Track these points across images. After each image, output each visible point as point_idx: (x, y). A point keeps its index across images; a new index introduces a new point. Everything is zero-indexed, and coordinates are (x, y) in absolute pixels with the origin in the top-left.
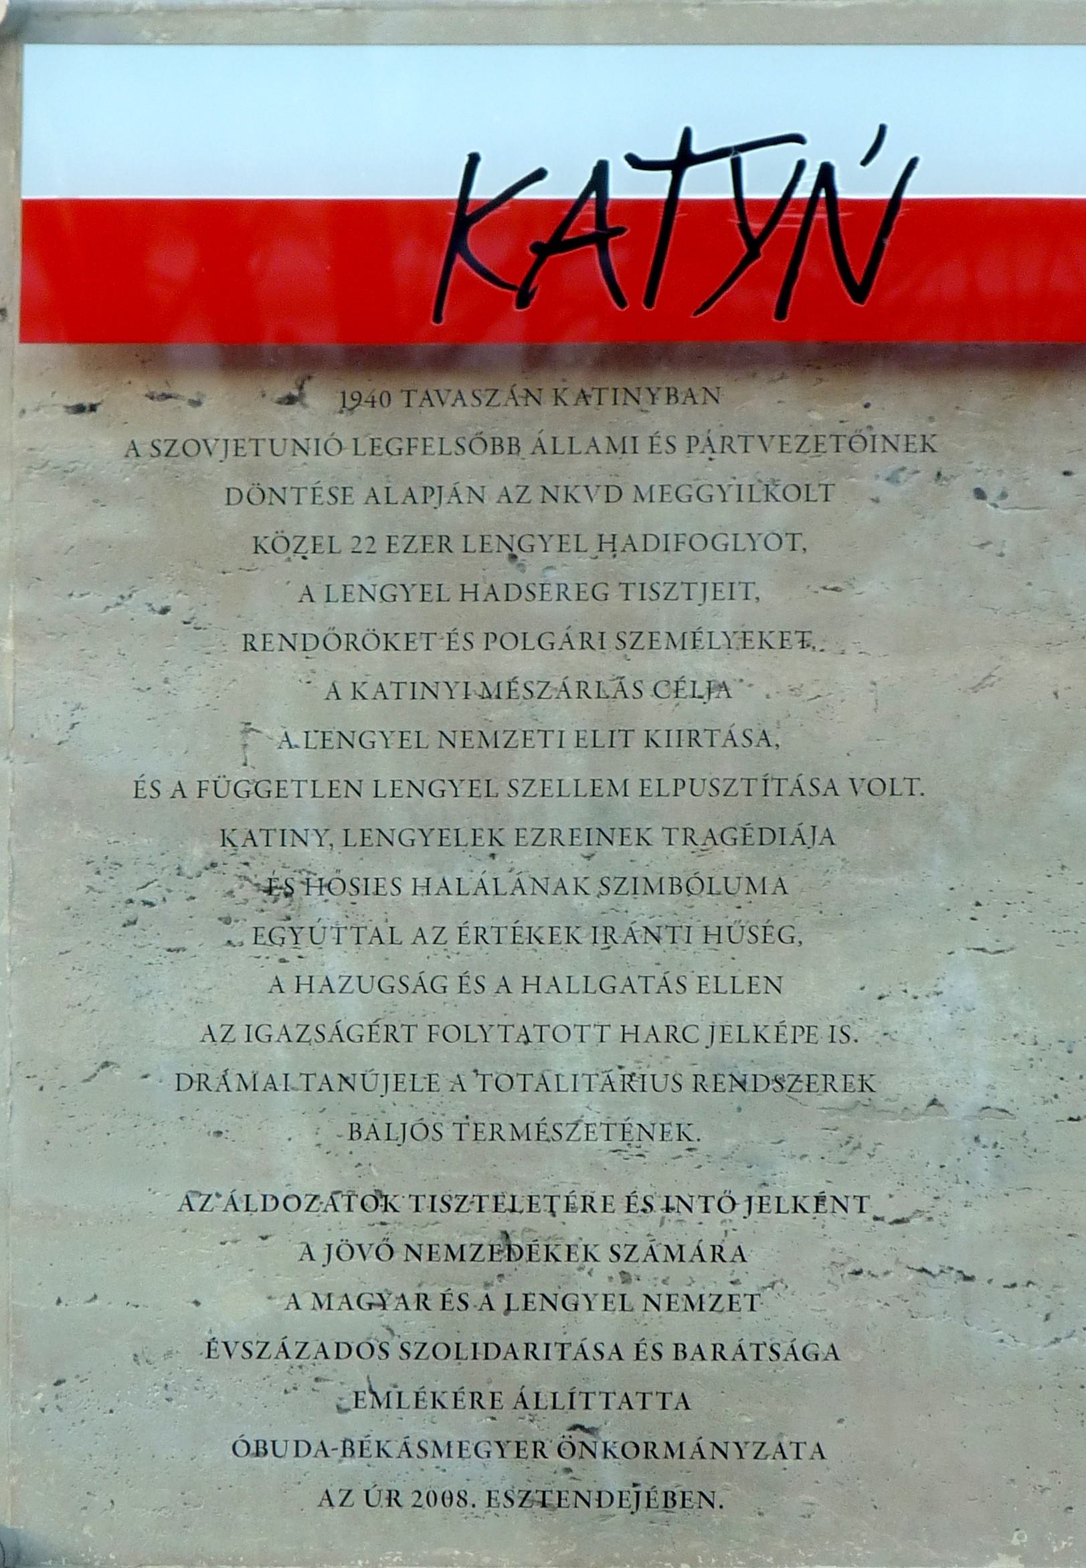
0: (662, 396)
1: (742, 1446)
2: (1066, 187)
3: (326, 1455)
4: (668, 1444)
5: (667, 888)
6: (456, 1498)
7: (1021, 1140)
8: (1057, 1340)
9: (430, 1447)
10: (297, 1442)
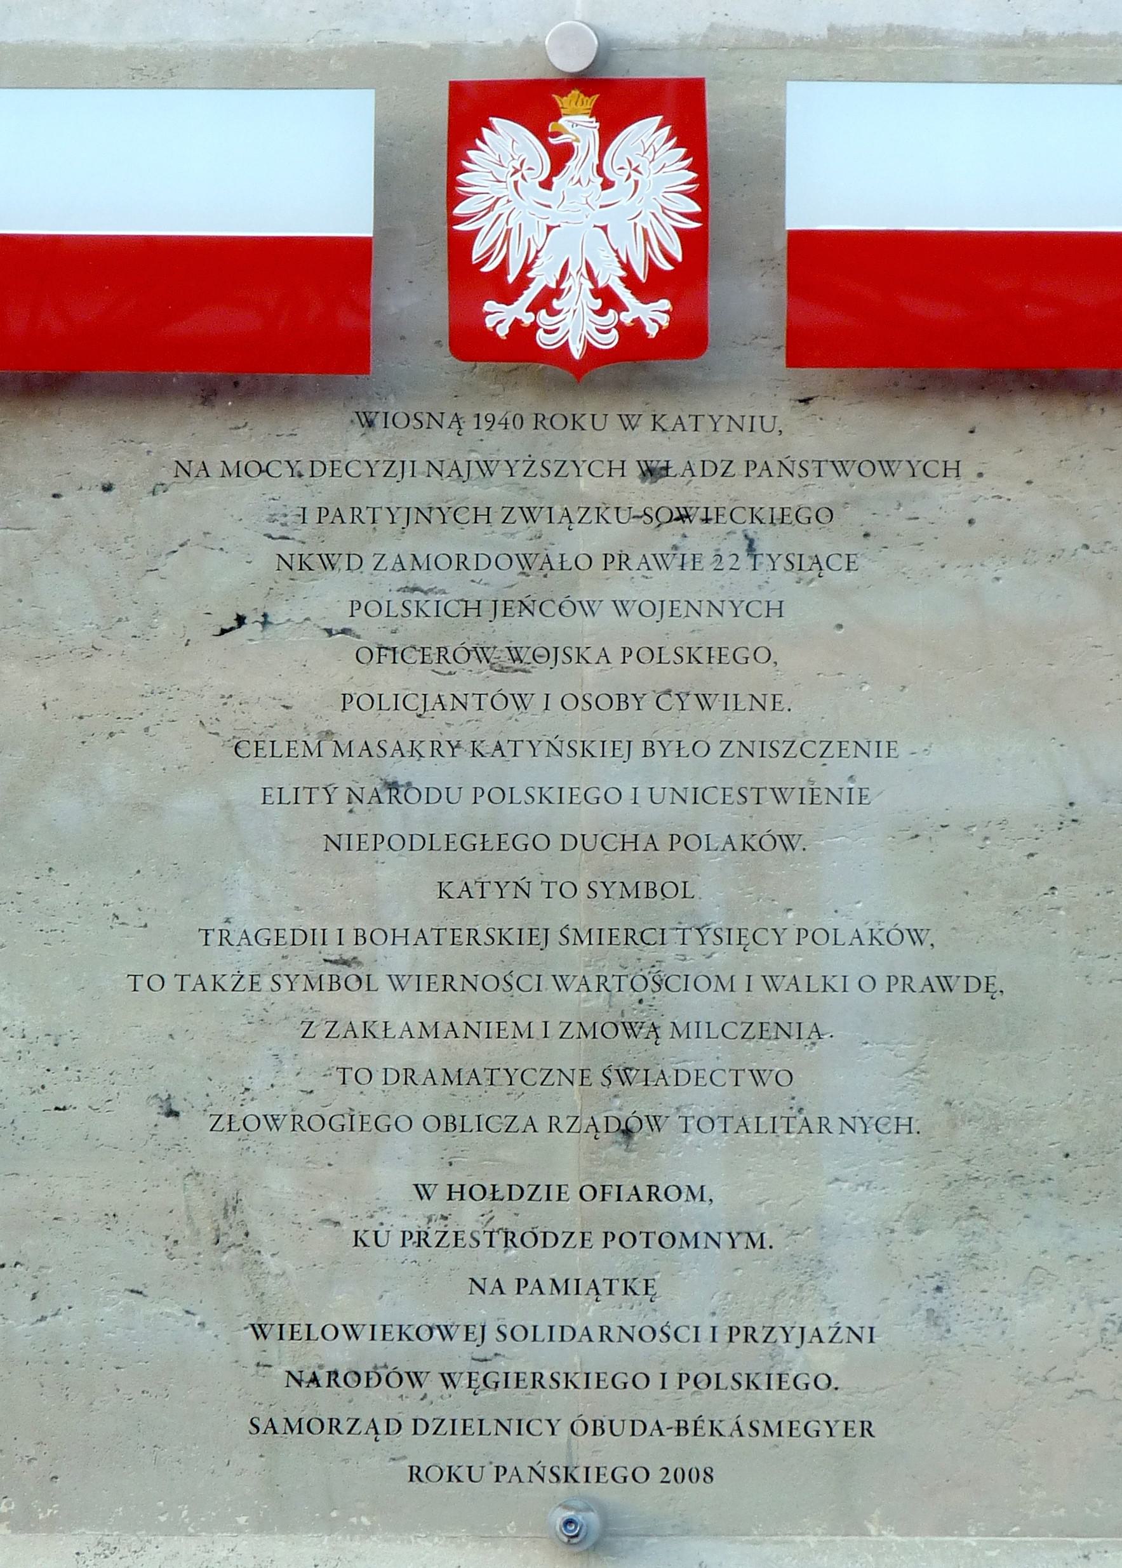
0: (646, 422)
1: (832, 1424)
2: (1102, 218)
3: (661, 1434)
4: (287, 1420)
5: (642, 892)
6: (702, 1475)
7: (10, 1128)
8: (43, 1318)
9: (761, 1427)
10: (633, 1422)
